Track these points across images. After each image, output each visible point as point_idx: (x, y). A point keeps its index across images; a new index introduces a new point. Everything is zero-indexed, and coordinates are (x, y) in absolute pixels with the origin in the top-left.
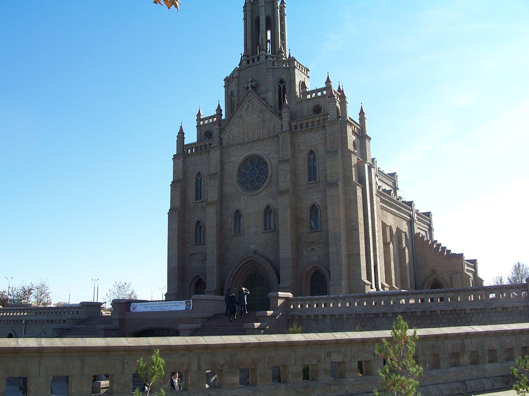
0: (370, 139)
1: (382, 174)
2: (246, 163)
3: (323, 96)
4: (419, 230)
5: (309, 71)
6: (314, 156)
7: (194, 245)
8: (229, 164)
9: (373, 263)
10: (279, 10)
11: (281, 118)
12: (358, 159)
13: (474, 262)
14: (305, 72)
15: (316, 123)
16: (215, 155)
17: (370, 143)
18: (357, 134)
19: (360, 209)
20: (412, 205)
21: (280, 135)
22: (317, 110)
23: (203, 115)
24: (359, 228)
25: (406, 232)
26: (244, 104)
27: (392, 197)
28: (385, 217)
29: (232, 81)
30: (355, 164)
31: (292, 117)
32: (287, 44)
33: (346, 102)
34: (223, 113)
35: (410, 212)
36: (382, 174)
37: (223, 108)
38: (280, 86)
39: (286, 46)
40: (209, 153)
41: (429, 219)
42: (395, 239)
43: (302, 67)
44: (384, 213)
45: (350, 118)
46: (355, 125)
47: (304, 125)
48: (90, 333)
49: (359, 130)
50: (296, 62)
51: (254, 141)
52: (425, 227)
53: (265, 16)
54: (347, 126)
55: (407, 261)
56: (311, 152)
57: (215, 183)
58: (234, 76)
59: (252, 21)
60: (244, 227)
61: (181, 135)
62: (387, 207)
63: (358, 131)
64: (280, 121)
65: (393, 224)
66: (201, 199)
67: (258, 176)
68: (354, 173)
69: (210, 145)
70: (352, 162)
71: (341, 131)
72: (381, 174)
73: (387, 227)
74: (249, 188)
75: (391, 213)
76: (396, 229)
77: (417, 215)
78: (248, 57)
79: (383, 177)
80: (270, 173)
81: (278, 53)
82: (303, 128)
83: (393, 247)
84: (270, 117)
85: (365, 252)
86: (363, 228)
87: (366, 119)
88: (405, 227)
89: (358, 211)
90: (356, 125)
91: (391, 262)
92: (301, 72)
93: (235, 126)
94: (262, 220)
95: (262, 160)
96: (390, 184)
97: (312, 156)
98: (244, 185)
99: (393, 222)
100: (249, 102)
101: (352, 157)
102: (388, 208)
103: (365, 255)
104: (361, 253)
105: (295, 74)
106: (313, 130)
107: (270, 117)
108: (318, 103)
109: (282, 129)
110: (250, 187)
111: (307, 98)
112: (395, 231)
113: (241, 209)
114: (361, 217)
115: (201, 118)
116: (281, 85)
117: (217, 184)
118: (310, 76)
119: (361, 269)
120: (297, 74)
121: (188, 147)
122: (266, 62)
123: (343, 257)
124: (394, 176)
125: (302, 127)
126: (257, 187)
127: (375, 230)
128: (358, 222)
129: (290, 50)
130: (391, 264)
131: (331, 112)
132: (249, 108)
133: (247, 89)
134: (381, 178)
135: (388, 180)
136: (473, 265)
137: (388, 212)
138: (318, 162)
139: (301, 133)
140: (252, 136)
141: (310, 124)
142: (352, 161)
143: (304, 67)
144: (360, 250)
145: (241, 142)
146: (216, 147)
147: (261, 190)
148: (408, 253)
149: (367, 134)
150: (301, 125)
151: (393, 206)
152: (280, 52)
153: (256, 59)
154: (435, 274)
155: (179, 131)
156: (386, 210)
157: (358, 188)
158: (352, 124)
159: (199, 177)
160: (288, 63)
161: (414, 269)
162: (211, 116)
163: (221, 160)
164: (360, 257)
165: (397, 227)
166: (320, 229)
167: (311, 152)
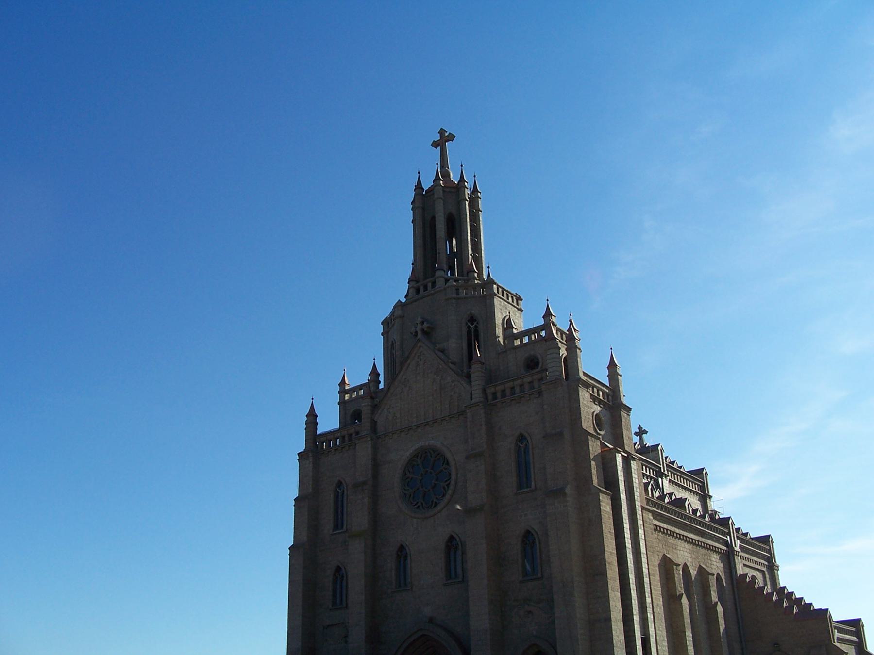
0: (629, 409)
1: (675, 472)
2: (415, 463)
3: (541, 340)
4: (749, 569)
5: (521, 300)
6: (526, 445)
9: (639, 634)
10: (467, 203)
11: (470, 382)
12: (602, 444)
13: (856, 626)
14: (513, 302)
15: (527, 387)
16: (364, 451)
17: (630, 416)
18: (605, 402)
19: (609, 535)
20: (729, 525)
21: (467, 411)
22: (532, 363)
23: (350, 383)
24: (607, 571)
25: (721, 574)
27: (687, 512)
28: (671, 549)
29: (394, 324)
30: (596, 454)
31: (490, 378)
32: (485, 259)
33: (576, 347)
34: (381, 378)
35: (726, 538)
36: (675, 472)
37: (381, 369)
38: (469, 327)
39: (483, 262)
40: (355, 448)
41: (768, 548)
42: (695, 589)
43: (507, 295)
44: (670, 541)
45: (585, 374)
46: (603, 390)
47: (508, 392)
49: (608, 396)
50: (495, 286)
51: (426, 424)
52: (759, 564)
54: (579, 388)
55: (722, 628)
56: (521, 438)
58: (396, 314)
59: (424, 224)
61: (312, 416)
62: (676, 529)
63: (606, 397)
65: (690, 560)
66: (342, 527)
67: (435, 483)
68: (594, 471)
69: (357, 433)
70: (589, 452)
72: (673, 473)
73: (675, 567)
74: (421, 507)
75: (686, 541)
76: (697, 569)
77: (740, 542)
78: (417, 282)
79: (679, 477)
80: (453, 477)
81: (468, 273)
82: (515, 394)
83: (688, 603)
84: (452, 382)
85: (621, 614)
86: (617, 570)
87: (621, 376)
88: (716, 565)
89: (605, 539)
90: (600, 386)
91: (685, 632)
95: (441, 456)
96: (694, 490)
97: (522, 444)
98: (412, 501)
99: (691, 558)
100: (418, 358)
101: (591, 443)
102: (677, 531)
103: (622, 620)
104: (612, 616)
105: (494, 306)
106: (523, 399)
107: (452, 382)
108: (532, 353)
109: (471, 400)
110: (422, 504)
111: (515, 345)
112: (695, 573)
113: (407, 544)
114: (611, 551)
115: (346, 388)
116: (471, 326)
118: (523, 309)
119: (613, 646)
120: (498, 305)
121: (322, 439)
122: (445, 289)
123: (579, 625)
124: (701, 475)
125: (504, 396)
126: (434, 503)
127: (643, 572)
128: (605, 560)
129: (489, 267)
130: (685, 634)
131: (550, 365)
132: (418, 368)
133: (414, 335)
134: (678, 481)
136: (853, 629)
137: (679, 540)
139: (504, 404)
141: (517, 390)
142: (591, 449)
143: (511, 293)
144: (610, 611)
145: (416, 424)
147: (439, 507)
148: (723, 611)
149: (622, 402)
150: (503, 391)
151: (688, 528)
152: (470, 272)
153: (429, 285)
154: (779, 651)
155: (308, 412)
156: (665, 532)
157: (602, 497)
158: (588, 385)
159: (340, 490)
160: (464, 289)
161: (741, 642)
162: (361, 385)
163: (374, 459)
164: (611, 624)
165: (700, 565)
166: (539, 576)
167: (521, 438)
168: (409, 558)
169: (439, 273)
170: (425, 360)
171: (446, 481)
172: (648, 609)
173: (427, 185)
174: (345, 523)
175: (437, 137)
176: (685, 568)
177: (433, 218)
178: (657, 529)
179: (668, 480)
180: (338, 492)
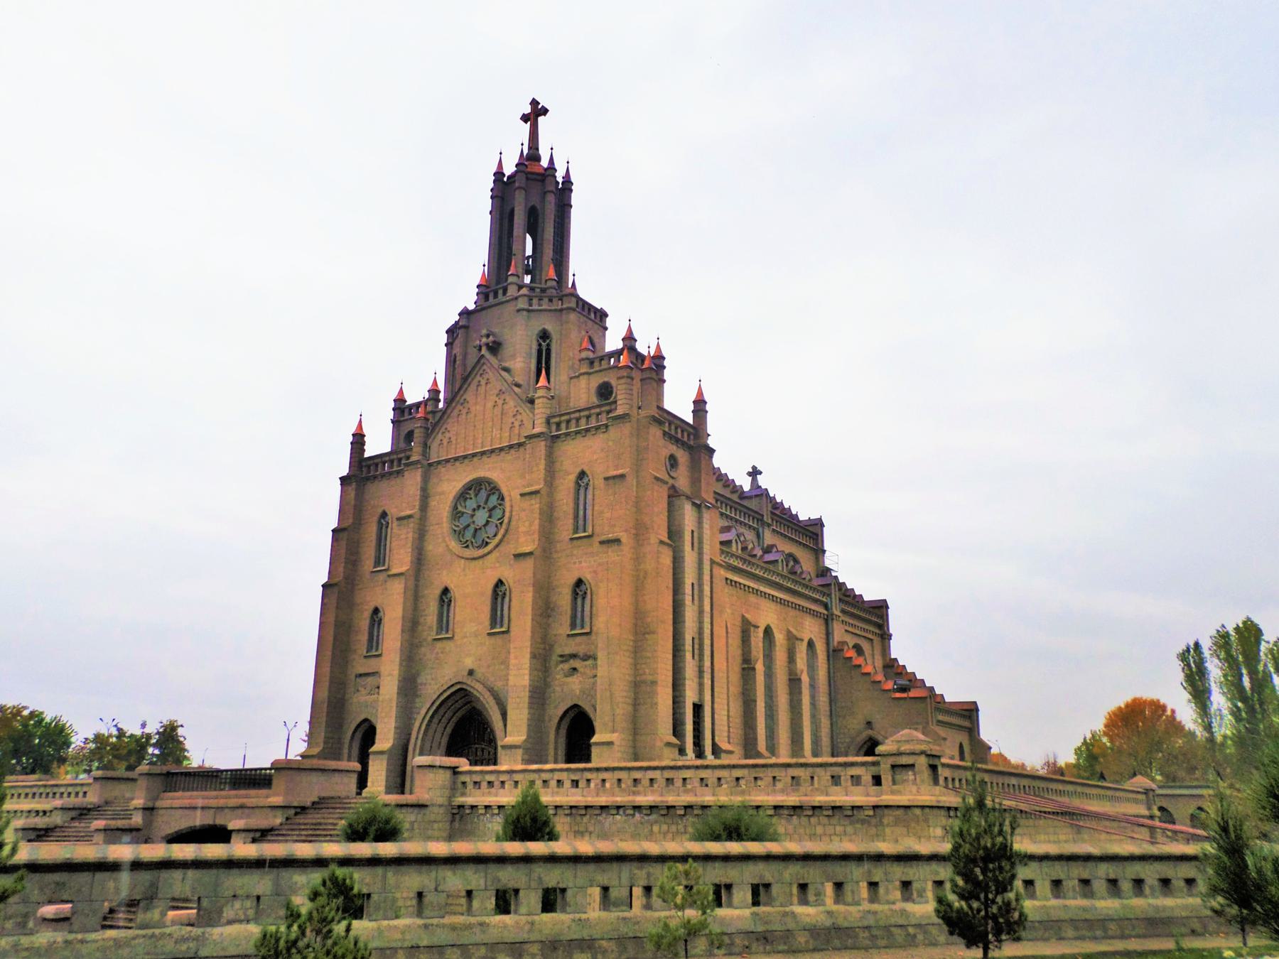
7: (365, 657)
23: (411, 399)
27: (780, 568)
34: (442, 396)
37: (441, 386)
48: (86, 839)
58: (460, 324)
61: (358, 440)
64: (531, 415)
73: (752, 629)
117: (410, 535)
121: (369, 463)
135: (796, 531)
146: (418, 462)
166: (587, 630)
167: (582, 474)
171: (499, 520)
173: (509, 169)
174: (387, 559)
175: (528, 110)
178: (728, 581)
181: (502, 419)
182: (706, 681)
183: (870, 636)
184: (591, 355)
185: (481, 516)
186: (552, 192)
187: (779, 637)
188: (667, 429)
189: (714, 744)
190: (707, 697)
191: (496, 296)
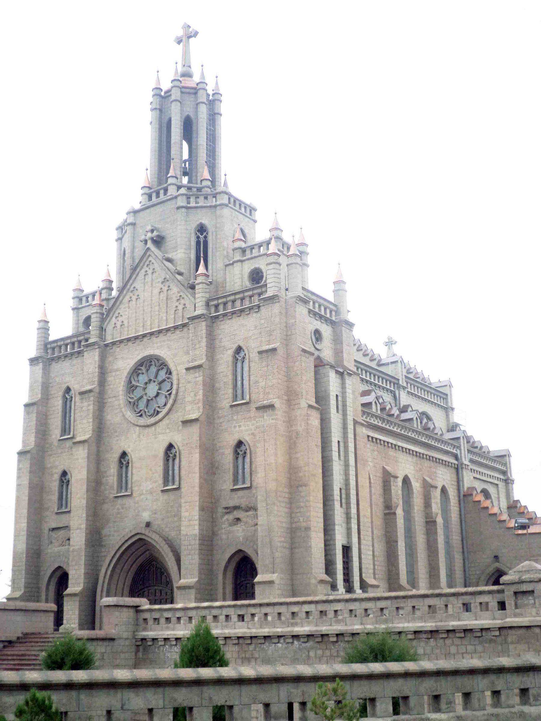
8: (114, 374)
26: (141, 270)
53: (181, 117)
57: (89, 405)
58: (128, 221)
60: (133, 481)
71: (286, 313)
73: (392, 479)
92: (237, 213)
93: (125, 308)
94: (160, 469)
95: (165, 366)
117: (91, 407)
138: (250, 367)
140: (149, 324)
166: (247, 485)
167: (239, 349)
168: (130, 465)
169: (170, 181)
170: (154, 269)
171: (168, 391)
172: (352, 520)
176: (406, 481)
177: (170, 120)
179: (406, 392)
180: (67, 398)
181: (167, 303)
182: (349, 440)
183: (496, 482)
184: (243, 245)
185: (152, 389)
186: (203, 103)
187: (416, 486)
188: (311, 308)
189: (362, 581)
190: (355, 540)
191: (158, 196)
